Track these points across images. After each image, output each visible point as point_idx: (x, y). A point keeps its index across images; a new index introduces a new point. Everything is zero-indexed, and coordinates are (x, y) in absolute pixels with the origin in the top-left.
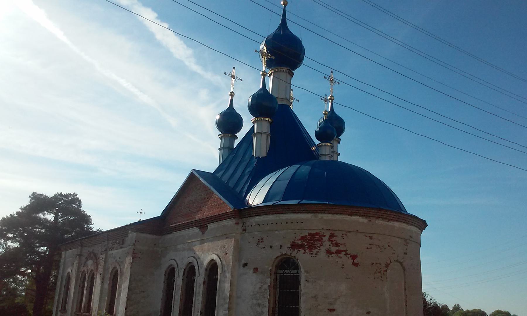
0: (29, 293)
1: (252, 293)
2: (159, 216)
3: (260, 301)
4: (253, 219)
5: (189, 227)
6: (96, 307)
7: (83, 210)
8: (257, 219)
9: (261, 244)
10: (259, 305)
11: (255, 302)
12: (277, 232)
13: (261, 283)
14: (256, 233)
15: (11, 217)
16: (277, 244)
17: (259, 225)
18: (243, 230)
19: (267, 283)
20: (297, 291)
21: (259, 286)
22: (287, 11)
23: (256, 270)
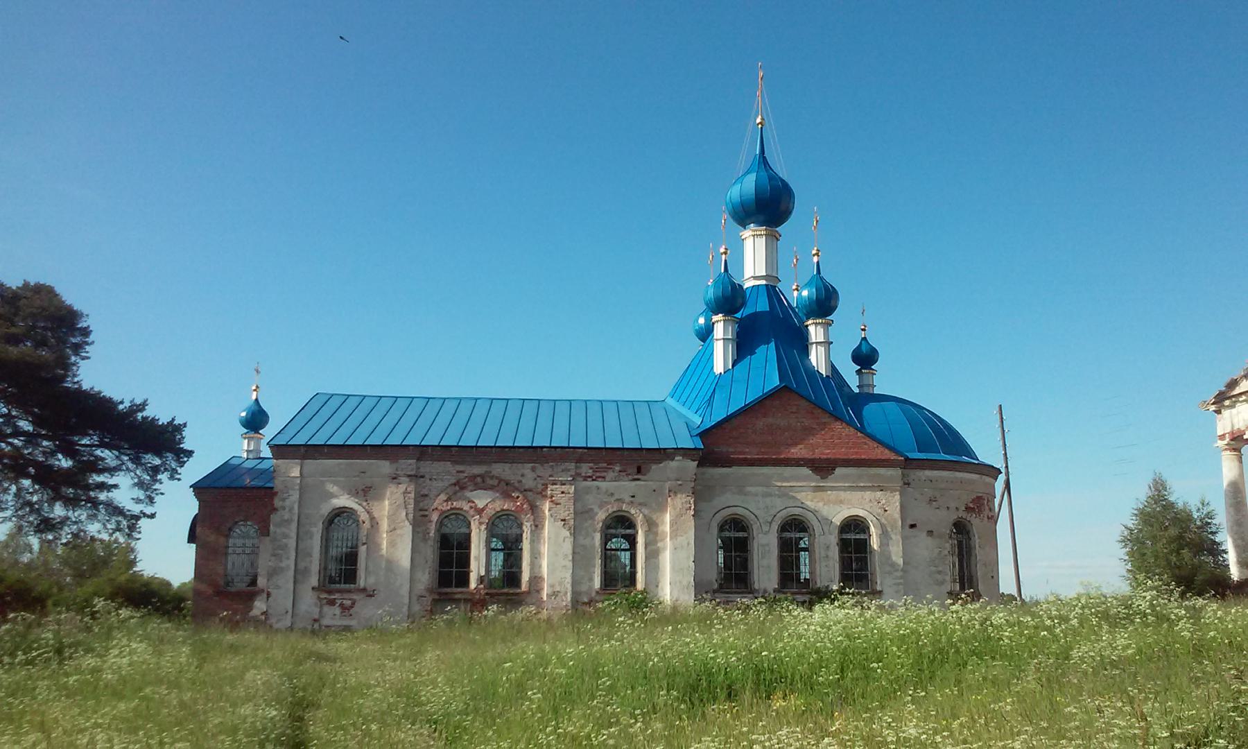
0: (714, 430)
1: (928, 560)
2: (199, 505)
3: (940, 569)
4: (922, 473)
5: (766, 465)
6: (295, 502)
7: (127, 404)
8: (928, 473)
9: (934, 503)
10: (939, 572)
11: (933, 569)
12: (951, 491)
13: (940, 548)
14: (926, 490)
15: (62, 453)
16: (953, 505)
17: (931, 481)
18: (905, 484)
19: (946, 549)
20: (12, 463)
21: (937, 551)
22: (384, 442)
23: (930, 533)
